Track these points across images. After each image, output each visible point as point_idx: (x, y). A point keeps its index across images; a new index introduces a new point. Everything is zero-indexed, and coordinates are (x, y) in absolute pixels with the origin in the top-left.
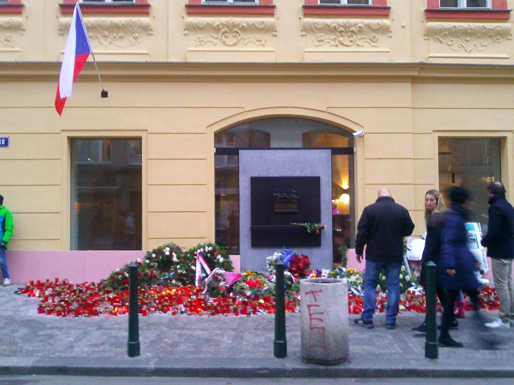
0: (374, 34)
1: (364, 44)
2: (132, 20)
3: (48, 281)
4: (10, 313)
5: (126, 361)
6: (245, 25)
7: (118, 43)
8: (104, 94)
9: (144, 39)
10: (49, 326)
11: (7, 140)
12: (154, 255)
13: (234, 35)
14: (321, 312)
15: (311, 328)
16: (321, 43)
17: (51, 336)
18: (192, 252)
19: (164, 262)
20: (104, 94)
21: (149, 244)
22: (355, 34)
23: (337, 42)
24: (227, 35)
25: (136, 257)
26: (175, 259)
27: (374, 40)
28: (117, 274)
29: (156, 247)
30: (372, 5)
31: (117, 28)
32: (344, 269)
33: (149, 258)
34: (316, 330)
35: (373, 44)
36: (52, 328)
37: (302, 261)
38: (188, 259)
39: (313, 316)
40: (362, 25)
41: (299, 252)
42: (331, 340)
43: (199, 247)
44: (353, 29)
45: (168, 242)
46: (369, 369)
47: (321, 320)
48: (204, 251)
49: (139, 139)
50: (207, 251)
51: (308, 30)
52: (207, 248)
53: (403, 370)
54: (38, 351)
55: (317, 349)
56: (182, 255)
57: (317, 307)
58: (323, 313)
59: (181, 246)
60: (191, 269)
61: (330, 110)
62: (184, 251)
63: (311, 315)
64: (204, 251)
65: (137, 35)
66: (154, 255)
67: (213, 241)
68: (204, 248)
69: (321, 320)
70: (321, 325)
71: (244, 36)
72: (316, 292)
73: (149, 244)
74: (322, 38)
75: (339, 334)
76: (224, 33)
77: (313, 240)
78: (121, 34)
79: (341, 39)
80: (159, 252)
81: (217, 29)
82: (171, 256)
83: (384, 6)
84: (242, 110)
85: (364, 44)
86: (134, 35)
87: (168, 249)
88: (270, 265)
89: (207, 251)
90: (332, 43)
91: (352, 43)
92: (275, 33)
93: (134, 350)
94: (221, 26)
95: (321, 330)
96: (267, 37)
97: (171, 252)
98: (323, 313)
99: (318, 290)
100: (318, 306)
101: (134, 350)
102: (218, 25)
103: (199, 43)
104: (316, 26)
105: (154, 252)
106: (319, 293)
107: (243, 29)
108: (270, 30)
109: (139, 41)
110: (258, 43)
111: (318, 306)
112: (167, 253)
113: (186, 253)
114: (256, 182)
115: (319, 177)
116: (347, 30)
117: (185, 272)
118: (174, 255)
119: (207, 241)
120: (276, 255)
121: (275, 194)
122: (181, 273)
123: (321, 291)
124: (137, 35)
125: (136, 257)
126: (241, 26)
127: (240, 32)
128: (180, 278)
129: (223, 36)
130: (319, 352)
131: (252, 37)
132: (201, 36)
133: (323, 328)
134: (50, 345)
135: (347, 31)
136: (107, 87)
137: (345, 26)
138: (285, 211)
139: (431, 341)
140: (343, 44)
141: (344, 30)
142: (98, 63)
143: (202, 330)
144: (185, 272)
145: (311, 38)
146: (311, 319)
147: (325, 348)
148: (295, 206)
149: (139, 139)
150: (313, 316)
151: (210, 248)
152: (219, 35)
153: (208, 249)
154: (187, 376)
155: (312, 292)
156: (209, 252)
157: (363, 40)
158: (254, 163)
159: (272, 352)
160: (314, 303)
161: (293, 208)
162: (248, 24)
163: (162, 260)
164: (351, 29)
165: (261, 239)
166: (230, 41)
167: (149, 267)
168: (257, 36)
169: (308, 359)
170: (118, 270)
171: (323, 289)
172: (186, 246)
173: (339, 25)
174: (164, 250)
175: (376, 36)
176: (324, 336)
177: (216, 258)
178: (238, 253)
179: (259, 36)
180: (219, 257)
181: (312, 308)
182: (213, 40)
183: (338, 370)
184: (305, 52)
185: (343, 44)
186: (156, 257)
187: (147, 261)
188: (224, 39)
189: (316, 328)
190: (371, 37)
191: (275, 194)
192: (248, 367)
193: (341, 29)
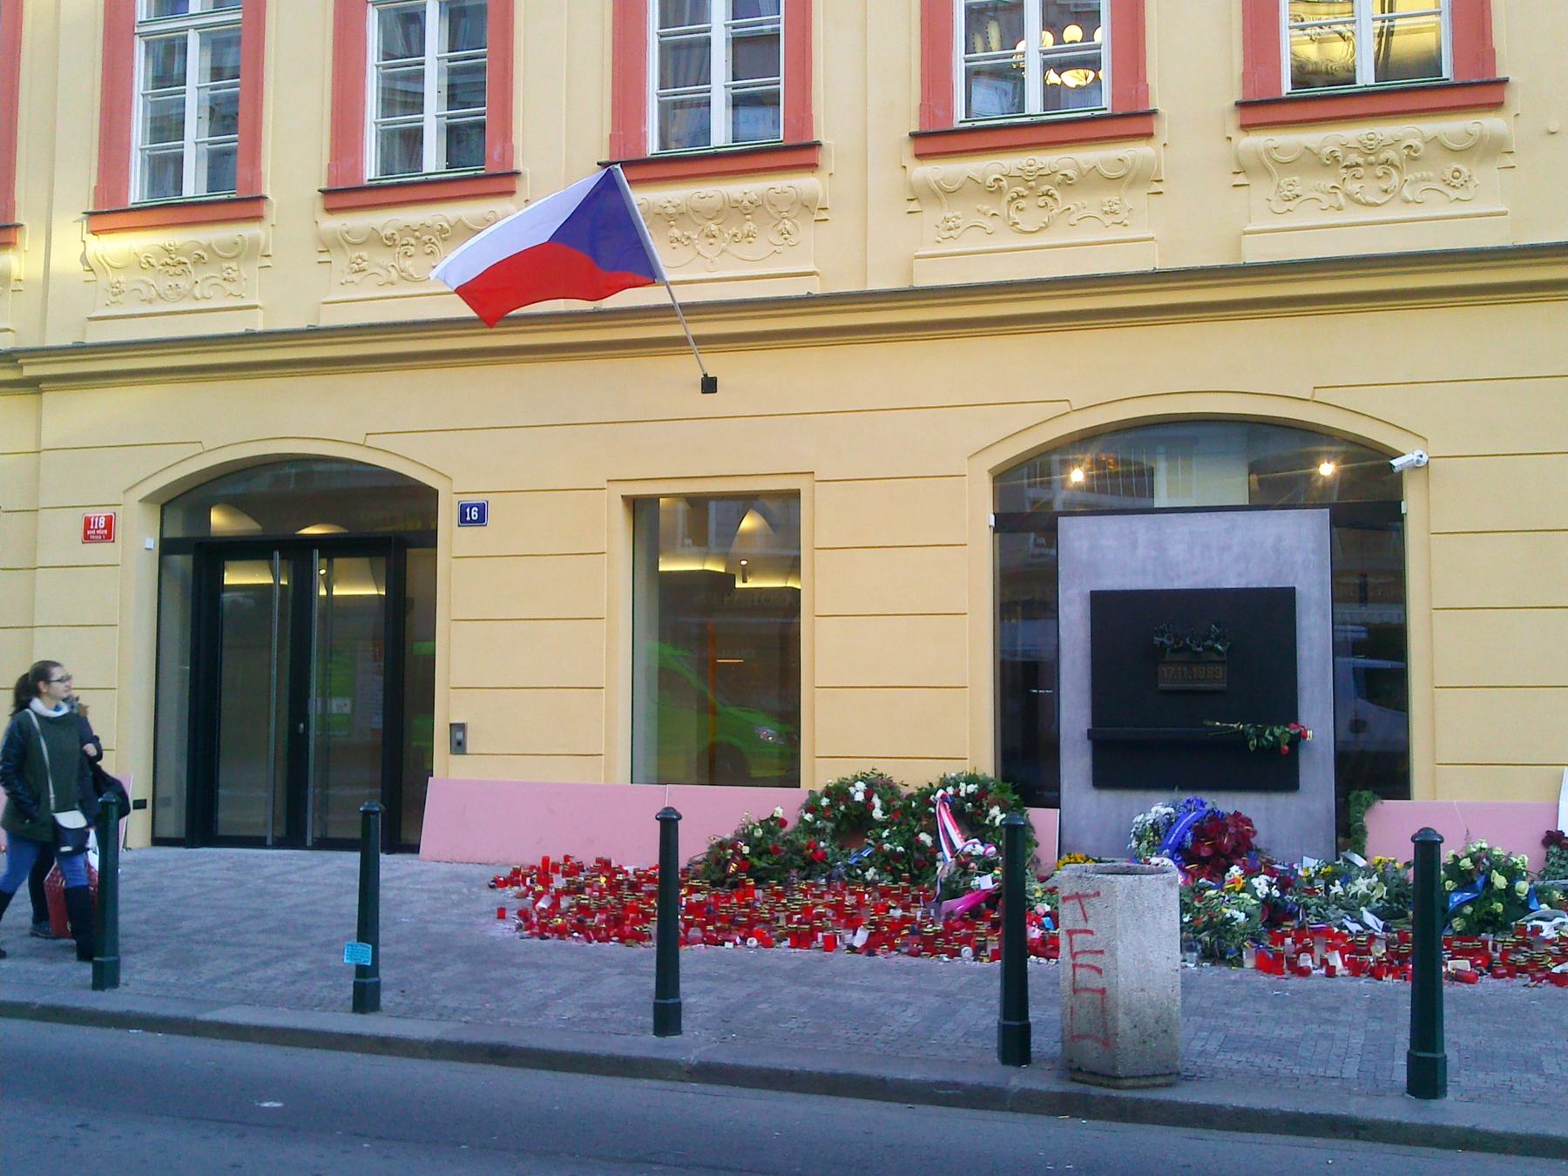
0: (1455, 166)
1: (1424, 196)
2: (1475, 129)
3: (567, 858)
4: (448, 928)
5: (647, 1044)
6: (1070, 173)
7: (742, 249)
8: (709, 385)
9: (805, 231)
10: (519, 960)
11: (482, 508)
12: (825, 802)
13: (1041, 202)
14: (1097, 948)
15: (1075, 991)
16: (1289, 205)
17: (511, 983)
18: (925, 796)
19: (845, 816)
20: (709, 385)
21: (818, 774)
22: (1395, 167)
23: (1340, 196)
24: (1022, 203)
25: (783, 804)
26: (877, 814)
27: (1455, 182)
28: (722, 845)
29: (832, 781)
30: (1452, 80)
31: (739, 210)
32: (1360, 861)
33: (810, 808)
34: (1086, 995)
35: (1454, 194)
36: (525, 965)
37: (1232, 830)
38: (913, 811)
39: (1080, 959)
40: (1415, 142)
41: (1226, 803)
42: (1123, 1023)
43: (944, 784)
44: (1390, 154)
45: (866, 767)
46: (1220, 1106)
47: (1099, 971)
48: (957, 794)
49: (795, 495)
50: (962, 794)
51: (923, 195)
52: (963, 785)
53: (1314, 1117)
54: (466, 1012)
55: (1088, 1043)
56: (898, 804)
57: (1089, 937)
58: (1101, 952)
59: (896, 781)
60: (918, 841)
61: (1321, 395)
62: (905, 791)
63: (1074, 955)
64: (957, 794)
65: (789, 225)
66: (825, 802)
67: (986, 765)
68: (956, 786)
69: (1099, 971)
70: (1099, 982)
71: (1063, 200)
72: (1088, 896)
73: (818, 774)
74: (1297, 191)
75: (1149, 1011)
76: (1013, 199)
77: (1276, 770)
78: (750, 226)
79: (1353, 187)
80: (839, 793)
81: (995, 191)
82: (867, 805)
83: (1275, 96)
84: (1065, 407)
85: (1424, 196)
86: (780, 227)
87: (861, 785)
88: (1140, 839)
89: (962, 794)
90: (1327, 201)
91: (1388, 197)
92: (1158, 187)
93: (667, 1018)
94: (1004, 183)
95: (1099, 996)
96: (1136, 199)
97: (868, 795)
98: (1101, 952)
99: (1090, 891)
100: (1091, 932)
101: (667, 1018)
102: (996, 180)
103: (947, 235)
104: (1276, 156)
105: (828, 792)
106: (1094, 900)
107: (1067, 183)
108: (1143, 179)
109: (793, 240)
110: (1108, 220)
111: (1091, 932)
112: (859, 797)
113: (910, 797)
114: (1104, 605)
115: (1291, 592)
116: (1372, 158)
117: (900, 849)
118: (876, 801)
119: (966, 768)
120: (1159, 808)
121: (1157, 640)
122: (893, 851)
123: (1098, 894)
124: (789, 225)
125: (783, 804)
126: (1059, 177)
127: (1057, 195)
128: (887, 862)
129: (1013, 206)
130: (1091, 1053)
131: (1087, 203)
132: (952, 211)
133: (1103, 991)
134: (499, 999)
135: (1373, 161)
136: (715, 364)
137: (1367, 150)
138: (1189, 686)
139: (1423, 1049)
140: (1358, 202)
141: (1361, 160)
142: (683, 307)
143: (866, 990)
144: (900, 849)
145: (1261, 191)
146: (1074, 966)
147: (1106, 1043)
148: (1221, 671)
149: (795, 495)
150: (1080, 959)
151: (972, 788)
152: (1002, 207)
153: (965, 789)
154: (770, 1087)
155: (1078, 896)
156: (969, 797)
157: (1423, 185)
158: (1106, 555)
159: (350, 925)
160: (1081, 926)
161: (1215, 677)
162: (1080, 170)
163: (844, 815)
164: (1382, 157)
165: (1118, 766)
166: (1031, 217)
167: (809, 829)
168: (1105, 199)
169: (1073, 1070)
170: (728, 836)
171: (1103, 889)
172: (911, 777)
173: (1348, 148)
174: (852, 790)
175: (1464, 169)
176: (1103, 1011)
177: (986, 814)
178: (1055, 803)
179: (1110, 197)
180: (995, 811)
181: (1077, 938)
182: (984, 221)
183: (1139, 1101)
184: (1245, 233)
185: (1358, 202)
186: (830, 806)
187: (808, 817)
188: (1016, 216)
189: (1087, 989)
190: (1448, 175)
191: (1157, 640)
192: (913, 1076)
193: (1354, 158)
